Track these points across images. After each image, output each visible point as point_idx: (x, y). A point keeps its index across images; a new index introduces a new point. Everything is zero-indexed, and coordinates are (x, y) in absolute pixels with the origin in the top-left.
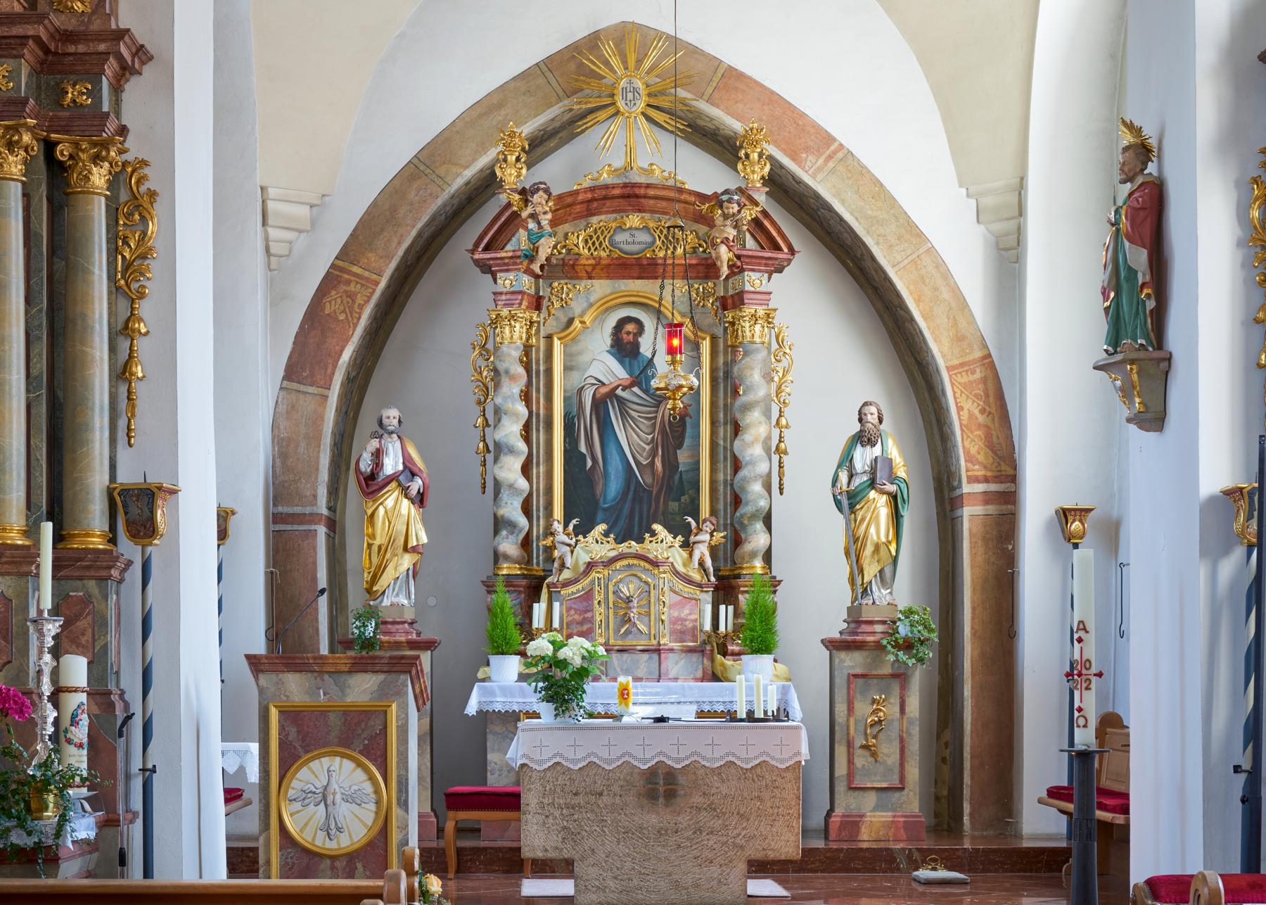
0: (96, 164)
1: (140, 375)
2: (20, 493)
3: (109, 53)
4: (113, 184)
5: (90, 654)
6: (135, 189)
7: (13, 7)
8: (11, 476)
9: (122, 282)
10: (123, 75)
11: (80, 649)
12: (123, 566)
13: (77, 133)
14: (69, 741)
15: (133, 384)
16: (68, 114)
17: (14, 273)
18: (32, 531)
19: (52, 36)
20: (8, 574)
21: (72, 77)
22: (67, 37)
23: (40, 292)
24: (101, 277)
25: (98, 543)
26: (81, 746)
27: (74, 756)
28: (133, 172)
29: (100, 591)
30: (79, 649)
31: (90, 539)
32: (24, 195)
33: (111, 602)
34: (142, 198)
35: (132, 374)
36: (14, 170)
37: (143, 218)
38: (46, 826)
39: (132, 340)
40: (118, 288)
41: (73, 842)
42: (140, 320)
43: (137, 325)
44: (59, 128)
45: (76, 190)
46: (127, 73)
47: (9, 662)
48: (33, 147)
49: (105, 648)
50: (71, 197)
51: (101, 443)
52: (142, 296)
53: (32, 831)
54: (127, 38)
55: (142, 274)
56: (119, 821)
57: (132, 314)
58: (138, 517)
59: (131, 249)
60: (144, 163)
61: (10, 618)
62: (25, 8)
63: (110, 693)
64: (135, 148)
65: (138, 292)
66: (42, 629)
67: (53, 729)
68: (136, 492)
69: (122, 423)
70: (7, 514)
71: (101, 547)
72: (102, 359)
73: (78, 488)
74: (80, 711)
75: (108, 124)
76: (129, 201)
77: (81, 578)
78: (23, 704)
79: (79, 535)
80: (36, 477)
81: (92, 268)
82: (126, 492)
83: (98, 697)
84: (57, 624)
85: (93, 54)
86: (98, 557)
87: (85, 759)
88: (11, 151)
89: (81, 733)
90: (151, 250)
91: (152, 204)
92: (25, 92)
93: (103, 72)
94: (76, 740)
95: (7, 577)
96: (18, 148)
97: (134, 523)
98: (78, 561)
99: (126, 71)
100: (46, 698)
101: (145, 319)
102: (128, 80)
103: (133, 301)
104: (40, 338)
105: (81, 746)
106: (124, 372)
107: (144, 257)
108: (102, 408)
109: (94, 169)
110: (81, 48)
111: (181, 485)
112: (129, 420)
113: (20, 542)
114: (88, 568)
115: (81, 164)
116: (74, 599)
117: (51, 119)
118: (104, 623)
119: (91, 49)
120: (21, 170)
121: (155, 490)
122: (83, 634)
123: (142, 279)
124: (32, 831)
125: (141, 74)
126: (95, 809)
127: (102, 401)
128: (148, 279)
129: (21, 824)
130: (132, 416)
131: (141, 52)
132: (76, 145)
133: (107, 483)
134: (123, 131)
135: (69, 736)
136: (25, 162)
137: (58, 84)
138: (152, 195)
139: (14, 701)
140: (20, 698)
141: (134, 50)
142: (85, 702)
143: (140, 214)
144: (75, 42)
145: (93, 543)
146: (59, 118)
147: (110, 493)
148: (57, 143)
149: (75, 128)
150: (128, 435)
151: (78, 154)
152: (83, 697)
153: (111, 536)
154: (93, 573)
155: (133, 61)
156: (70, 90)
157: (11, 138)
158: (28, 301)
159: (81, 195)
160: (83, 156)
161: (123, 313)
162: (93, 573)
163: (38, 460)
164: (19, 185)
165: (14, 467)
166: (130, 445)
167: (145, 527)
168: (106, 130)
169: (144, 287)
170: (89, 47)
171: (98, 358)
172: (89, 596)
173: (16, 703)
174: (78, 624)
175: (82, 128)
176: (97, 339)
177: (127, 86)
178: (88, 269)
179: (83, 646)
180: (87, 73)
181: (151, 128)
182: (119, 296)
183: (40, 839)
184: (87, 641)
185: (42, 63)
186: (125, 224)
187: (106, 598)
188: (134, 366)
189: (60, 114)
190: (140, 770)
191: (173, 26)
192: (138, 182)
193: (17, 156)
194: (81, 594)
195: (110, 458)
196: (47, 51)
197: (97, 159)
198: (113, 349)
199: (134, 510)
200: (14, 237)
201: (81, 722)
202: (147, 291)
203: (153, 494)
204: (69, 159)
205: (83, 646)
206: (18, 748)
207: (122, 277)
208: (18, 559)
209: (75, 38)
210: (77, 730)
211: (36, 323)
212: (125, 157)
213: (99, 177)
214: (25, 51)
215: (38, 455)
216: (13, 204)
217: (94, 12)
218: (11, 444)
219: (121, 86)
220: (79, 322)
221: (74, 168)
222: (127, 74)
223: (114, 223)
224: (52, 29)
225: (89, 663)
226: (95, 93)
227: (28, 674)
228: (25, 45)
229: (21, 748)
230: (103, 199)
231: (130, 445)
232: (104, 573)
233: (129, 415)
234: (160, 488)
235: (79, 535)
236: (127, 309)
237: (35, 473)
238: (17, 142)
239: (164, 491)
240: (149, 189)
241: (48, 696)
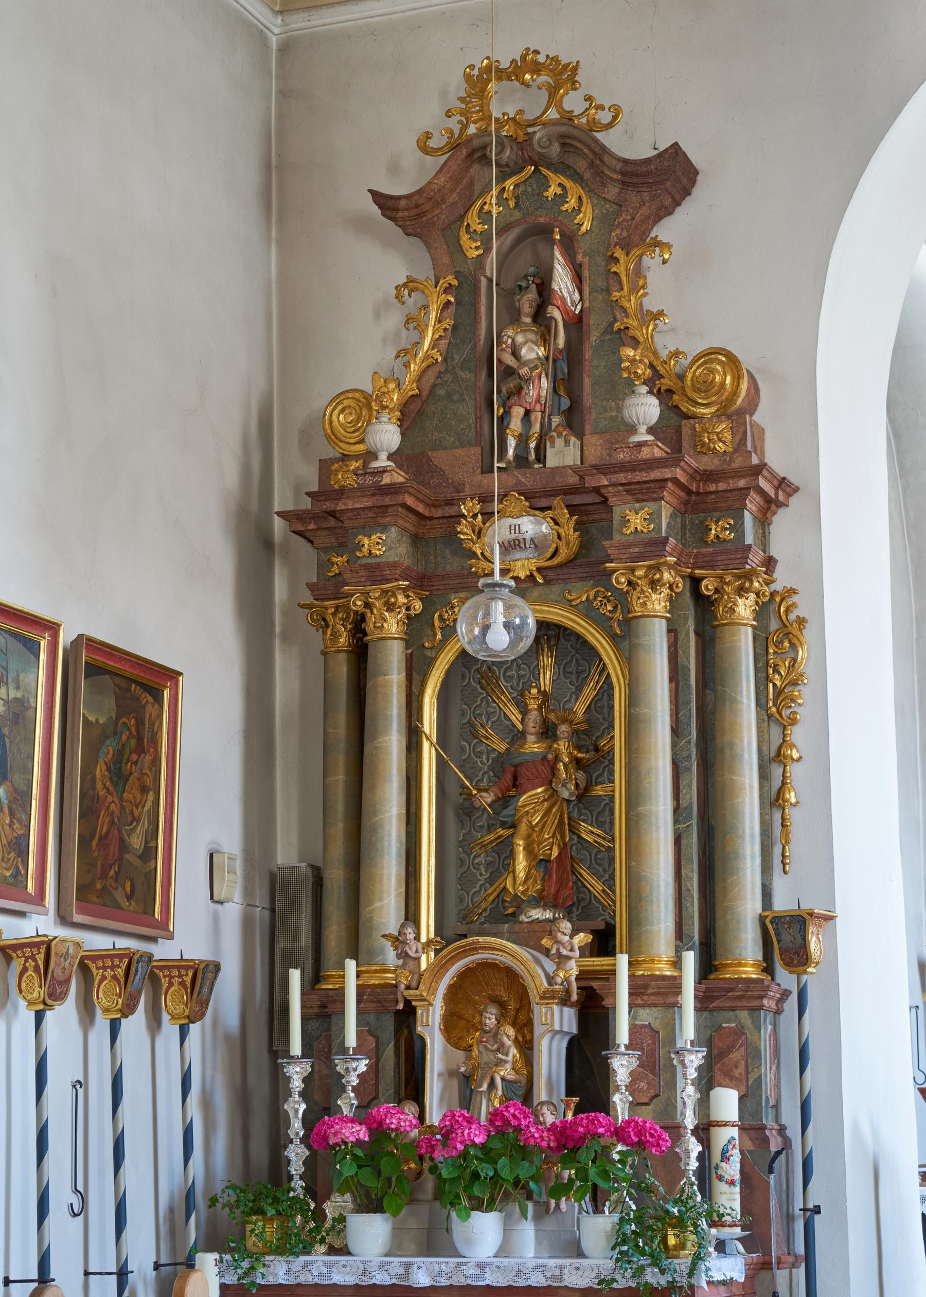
0: (741, 596)
1: (793, 800)
2: (668, 924)
3: (750, 488)
4: (762, 612)
5: (743, 1088)
6: (784, 617)
7: (654, 454)
8: (659, 907)
9: (774, 709)
10: (769, 508)
11: (734, 1082)
12: (778, 995)
13: (721, 567)
14: (720, 1178)
15: (787, 811)
16: (712, 549)
17: (659, 707)
18: (677, 963)
19: (692, 477)
20: (654, 1005)
21: (715, 514)
22: (708, 476)
23: (689, 724)
24: (749, 706)
25: (751, 972)
26: (732, 1183)
27: (726, 1193)
28: (782, 600)
29: (753, 1022)
30: (731, 1081)
31: (742, 969)
32: (669, 631)
33: (765, 1033)
34: (791, 625)
35: (785, 801)
36: (657, 607)
37: (793, 646)
38: (680, 1264)
39: (785, 766)
40: (770, 716)
41: (709, 1283)
42: (792, 746)
43: (789, 752)
44: (704, 564)
45: (721, 622)
46: (773, 506)
47: (657, 1096)
48: (677, 584)
49: (759, 1080)
50: (635, 621)
51: (752, 870)
52: (793, 722)
53: (665, 1269)
54: (765, 472)
55: (793, 701)
56: (772, 1264)
57: (784, 741)
58: (791, 944)
59: (782, 676)
60: (792, 592)
61: (657, 1050)
62: (667, 453)
63: (764, 1128)
64: (782, 579)
65: (790, 718)
66: (684, 1060)
67: (697, 1164)
68: (788, 919)
69: (777, 850)
70: (655, 945)
71: (754, 976)
72: (751, 787)
73: (729, 917)
74: (731, 1147)
75: (751, 556)
76: (779, 629)
77: (733, 1009)
78: (659, 1137)
79: (731, 965)
80: (687, 908)
81: (738, 697)
82: (778, 920)
83: (752, 1131)
84: (700, 1055)
85: (734, 490)
86: (749, 987)
87: (738, 1197)
88: (654, 590)
89: (732, 1169)
90: (802, 675)
91: (801, 630)
92: (667, 532)
93: (744, 507)
94: (727, 1177)
95: (654, 1009)
96: (661, 586)
97: (787, 951)
98: (730, 992)
99: (770, 505)
100: (689, 1132)
101: (797, 744)
102: (775, 513)
103: (785, 728)
104: (689, 769)
105: (732, 1183)
106: (777, 799)
107: (795, 683)
108: (752, 836)
109: (740, 600)
110: (722, 486)
111: (839, 911)
112: (784, 848)
113: (668, 973)
114: (739, 998)
115: (726, 597)
116: (727, 1030)
117: (696, 556)
118: (757, 1055)
119: (732, 486)
120: (666, 606)
121: (806, 916)
122: (736, 1067)
123: (793, 705)
124: (665, 1269)
125: (788, 506)
126: (749, 1250)
127: (752, 829)
128: (800, 705)
129: (655, 1263)
130: (786, 842)
131: (782, 483)
132: (721, 578)
133: (759, 911)
134: (770, 563)
135: (719, 1172)
136: (670, 599)
137: (702, 522)
138: (801, 621)
139: (650, 1133)
140: (656, 1131)
141: (776, 483)
142: (736, 1136)
143: (790, 642)
144: (716, 481)
145: (745, 972)
146: (704, 555)
147: (762, 920)
148: (702, 579)
149: (719, 563)
150: (782, 862)
151: (723, 588)
152: (734, 1132)
153: (765, 965)
154: (745, 1003)
155: (777, 494)
156: (714, 527)
157: (653, 577)
158: (676, 731)
159: (727, 627)
160: (728, 589)
161: (776, 740)
162: (745, 1003)
163: (689, 890)
164: (664, 621)
165: (661, 897)
166: (785, 872)
167: (798, 955)
168: (749, 562)
169: (795, 713)
170: (729, 484)
171: (747, 786)
172: (743, 1027)
173: (652, 1135)
174: (731, 1056)
175: (725, 562)
176: (746, 768)
177: (775, 519)
178: (736, 698)
179: (736, 1079)
180: (729, 508)
181: (799, 557)
182: (772, 724)
183: (674, 1279)
184: (741, 1074)
185: (686, 504)
186: (775, 653)
187: (758, 1029)
188: (787, 792)
189: (704, 550)
190: (800, 1210)
191: (818, 457)
192: (787, 611)
193: (660, 594)
194: (734, 1025)
195: (763, 885)
196: (689, 492)
197: (741, 591)
198: (764, 775)
199: (787, 938)
200: (658, 671)
201: (732, 1158)
202: (798, 717)
203: (805, 920)
204: (714, 593)
205: (736, 1079)
206: (653, 1183)
207: (774, 705)
208: (664, 990)
209: (715, 477)
210: (728, 1166)
211: (685, 754)
212: (773, 587)
213: (745, 608)
214: (665, 493)
215: (689, 885)
216: (657, 640)
217: (735, 450)
218: (658, 875)
219: (767, 518)
220: (727, 751)
221: (720, 602)
222: (773, 507)
223: (765, 652)
224: (691, 471)
225: (741, 1099)
226: (739, 527)
227: (676, 1107)
228: (665, 488)
229: (656, 1183)
230: (750, 630)
231: (785, 872)
232: (756, 1003)
233: (783, 842)
234: (811, 915)
235: (731, 965)
236: (780, 736)
237: (686, 904)
238: (659, 580)
239: (818, 917)
240: (798, 616)
241: (691, 1130)
